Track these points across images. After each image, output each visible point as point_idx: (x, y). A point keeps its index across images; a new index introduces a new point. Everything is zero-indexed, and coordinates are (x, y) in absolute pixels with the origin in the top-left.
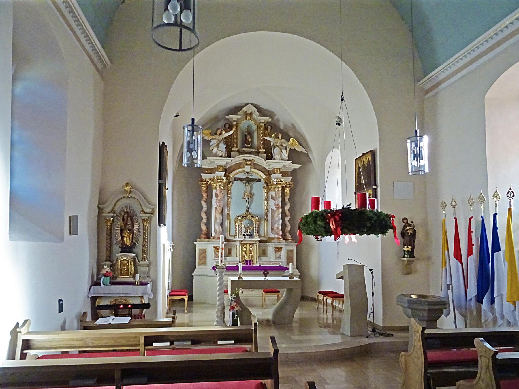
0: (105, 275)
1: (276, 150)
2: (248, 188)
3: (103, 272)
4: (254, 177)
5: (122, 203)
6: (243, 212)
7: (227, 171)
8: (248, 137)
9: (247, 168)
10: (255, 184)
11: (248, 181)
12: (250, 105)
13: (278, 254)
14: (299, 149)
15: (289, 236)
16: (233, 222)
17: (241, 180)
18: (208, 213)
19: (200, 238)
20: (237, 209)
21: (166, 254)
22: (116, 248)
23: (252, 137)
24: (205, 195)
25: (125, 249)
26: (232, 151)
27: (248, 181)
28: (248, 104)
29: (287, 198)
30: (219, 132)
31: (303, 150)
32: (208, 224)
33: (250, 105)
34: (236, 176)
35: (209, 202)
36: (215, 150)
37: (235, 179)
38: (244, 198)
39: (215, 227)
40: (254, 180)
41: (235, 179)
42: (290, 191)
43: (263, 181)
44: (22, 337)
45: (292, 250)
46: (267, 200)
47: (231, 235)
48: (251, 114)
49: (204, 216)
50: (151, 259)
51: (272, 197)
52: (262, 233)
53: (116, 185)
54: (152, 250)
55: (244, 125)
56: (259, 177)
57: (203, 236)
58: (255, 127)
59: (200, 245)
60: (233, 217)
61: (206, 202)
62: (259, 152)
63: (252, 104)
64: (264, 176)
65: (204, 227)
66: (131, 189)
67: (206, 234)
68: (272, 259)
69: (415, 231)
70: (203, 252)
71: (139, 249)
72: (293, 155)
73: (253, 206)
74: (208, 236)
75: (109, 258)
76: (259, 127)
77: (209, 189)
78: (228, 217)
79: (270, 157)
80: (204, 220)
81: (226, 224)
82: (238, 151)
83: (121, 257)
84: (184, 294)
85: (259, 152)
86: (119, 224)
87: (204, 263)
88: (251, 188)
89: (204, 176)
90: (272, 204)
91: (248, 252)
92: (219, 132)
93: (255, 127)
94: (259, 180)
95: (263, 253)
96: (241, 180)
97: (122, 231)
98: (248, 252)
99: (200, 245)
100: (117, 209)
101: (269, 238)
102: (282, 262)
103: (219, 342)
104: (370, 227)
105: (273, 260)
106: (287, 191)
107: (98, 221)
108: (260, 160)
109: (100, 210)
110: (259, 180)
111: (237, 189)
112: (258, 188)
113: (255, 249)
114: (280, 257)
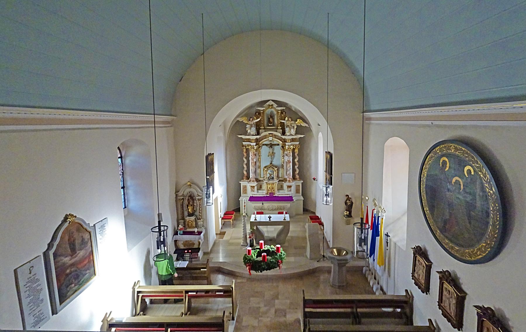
0: (180, 230)
1: (287, 129)
2: (271, 150)
3: (179, 228)
4: (275, 143)
5: (188, 190)
6: (268, 164)
7: (257, 141)
8: (271, 119)
10: (276, 147)
11: (271, 146)
13: (289, 189)
14: (304, 124)
15: (297, 176)
16: (262, 170)
17: (266, 145)
18: (248, 165)
19: (243, 179)
20: (265, 162)
22: (186, 213)
23: (273, 119)
24: (245, 154)
25: (190, 215)
26: (260, 129)
27: (271, 146)
29: (296, 154)
30: (251, 119)
31: (307, 125)
32: (248, 171)
35: (248, 158)
36: (249, 131)
37: (263, 145)
39: (251, 175)
40: (275, 145)
41: (263, 145)
42: (299, 150)
44: (136, 290)
45: (299, 185)
46: (283, 156)
47: (193, 300)
48: (272, 105)
49: (245, 166)
50: (204, 218)
51: (287, 155)
52: (280, 175)
53: (184, 180)
54: (204, 212)
55: (268, 111)
57: (245, 178)
58: (275, 113)
59: (243, 183)
60: (262, 166)
61: (246, 158)
62: (277, 129)
63: (273, 100)
64: (281, 143)
65: (245, 173)
66: (192, 184)
67: (247, 177)
68: (285, 193)
69: (352, 203)
70: (245, 187)
71: (197, 213)
72: (299, 130)
73: (274, 160)
74: (248, 178)
75: (183, 218)
76: (278, 113)
77: (248, 151)
78: (259, 167)
79: (284, 133)
80: (245, 169)
81: (258, 171)
82: (264, 129)
83: (187, 219)
85: (277, 129)
86: (186, 202)
87: (246, 193)
88: (273, 150)
89: (244, 143)
90: (286, 158)
92: (251, 119)
93: (275, 113)
94: (278, 145)
95: (281, 188)
96: (266, 145)
97: (188, 206)
99: (243, 183)
100: (185, 194)
101: (285, 179)
102: (292, 193)
103: (217, 293)
105: (286, 193)
106: (296, 151)
107: (176, 201)
109: (177, 191)
110: (278, 145)
111: (265, 150)
112: (278, 150)
113: (276, 187)
114: (290, 191)
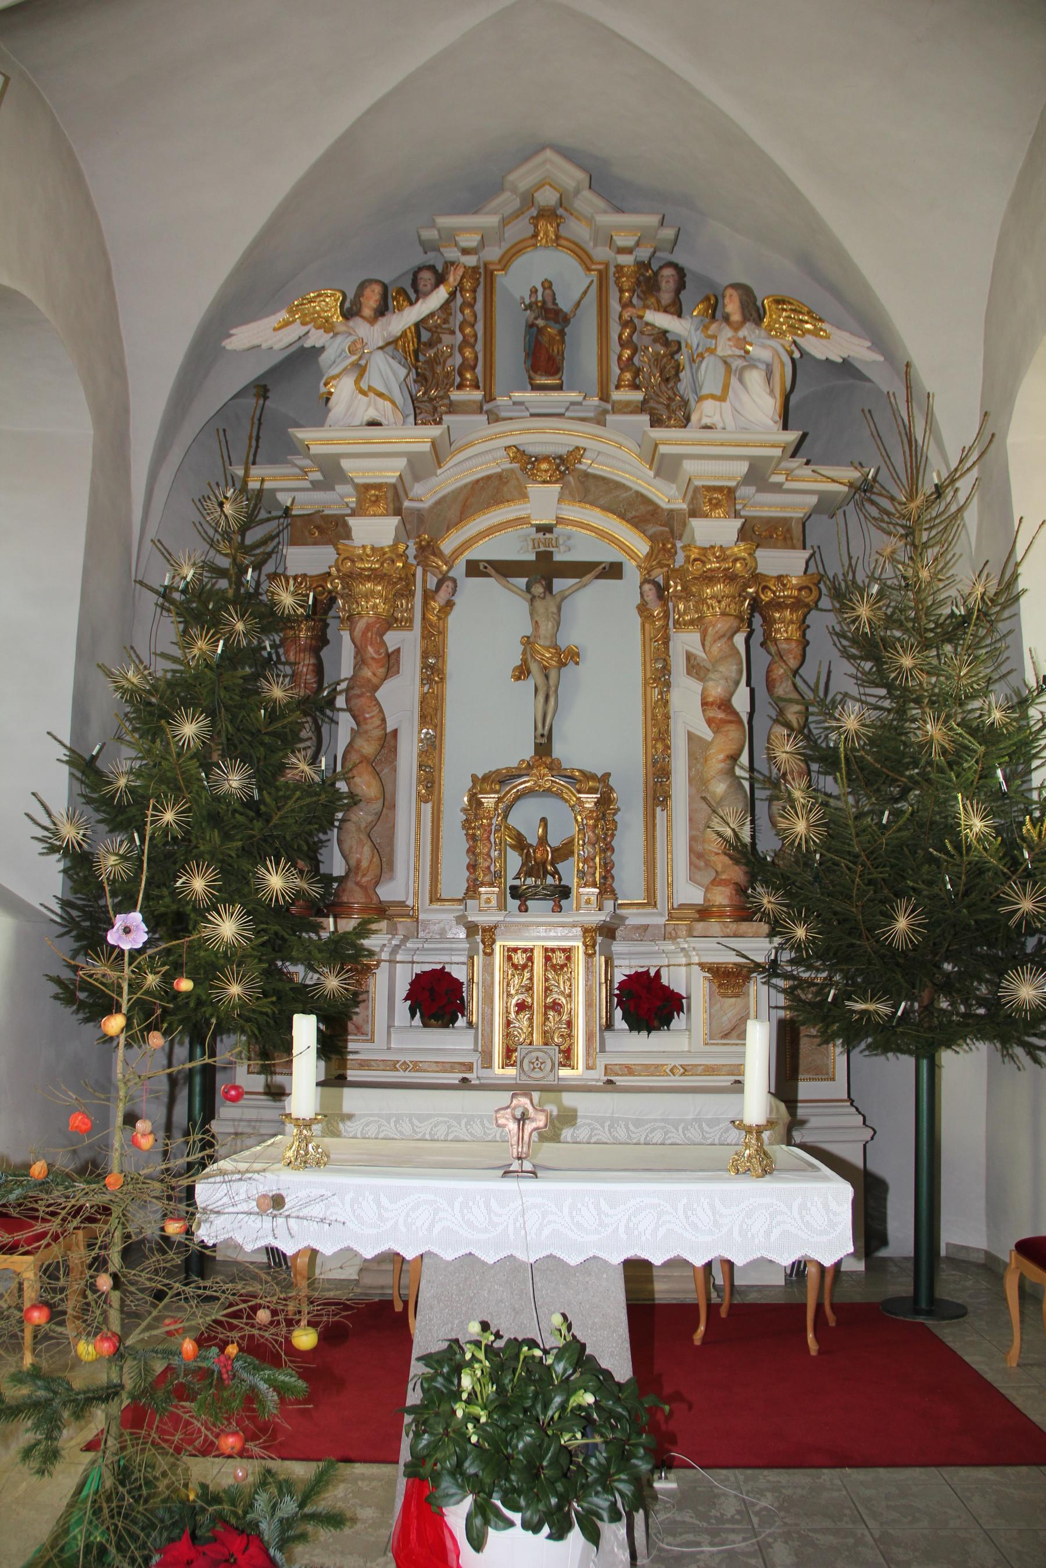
9: (543, 501)
11: (543, 573)
12: (548, 153)
17: (505, 569)
21: (255, 1111)
28: (543, 148)
33: (548, 153)
34: (481, 552)
37: (474, 569)
38: (522, 672)
40: (580, 570)
43: (632, 574)
56: (608, 555)
84: (122, 842)
91: (537, 999)
94: (614, 571)
98: (537, 999)
104: (153, 921)
108: (617, 452)
110: (614, 571)
112: (604, 623)
